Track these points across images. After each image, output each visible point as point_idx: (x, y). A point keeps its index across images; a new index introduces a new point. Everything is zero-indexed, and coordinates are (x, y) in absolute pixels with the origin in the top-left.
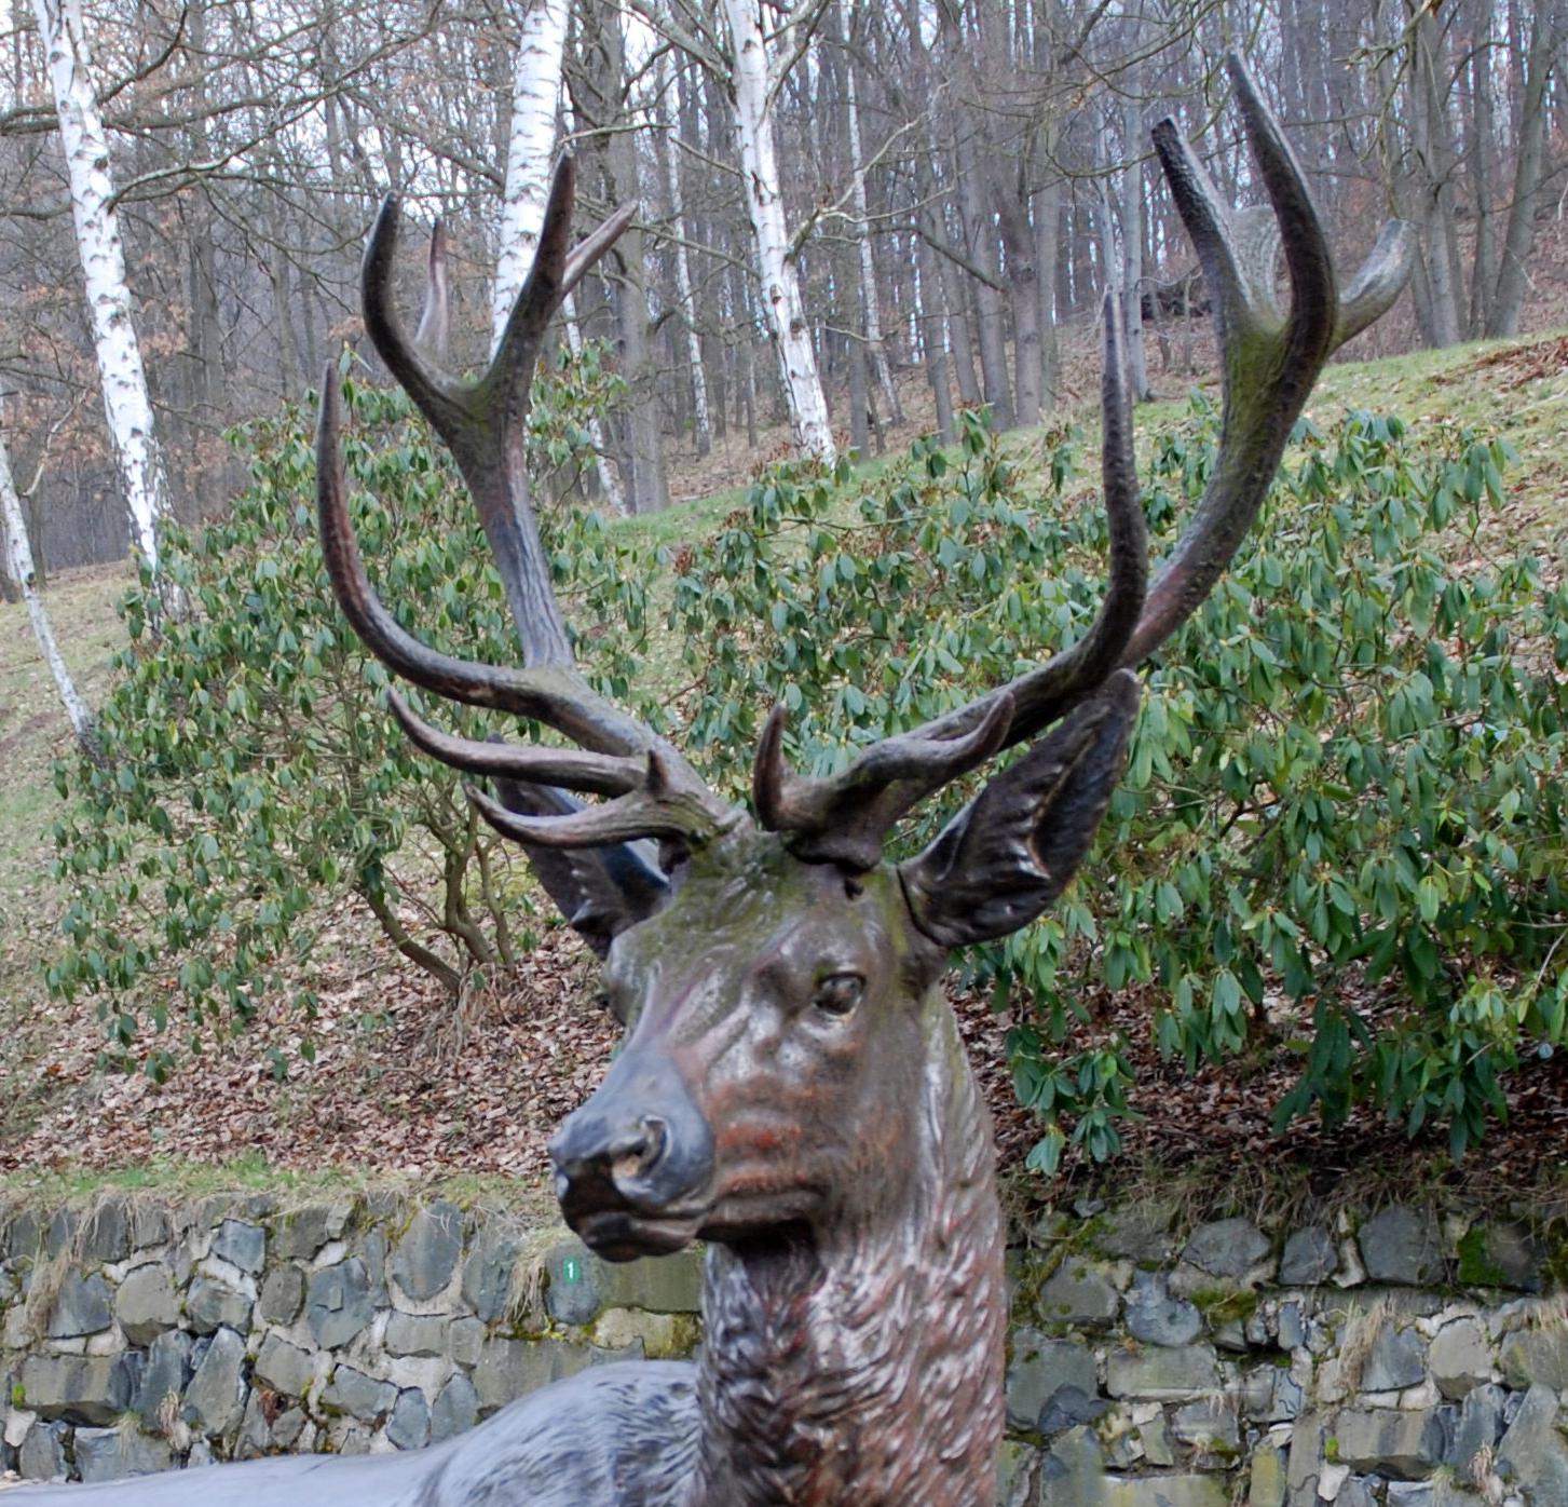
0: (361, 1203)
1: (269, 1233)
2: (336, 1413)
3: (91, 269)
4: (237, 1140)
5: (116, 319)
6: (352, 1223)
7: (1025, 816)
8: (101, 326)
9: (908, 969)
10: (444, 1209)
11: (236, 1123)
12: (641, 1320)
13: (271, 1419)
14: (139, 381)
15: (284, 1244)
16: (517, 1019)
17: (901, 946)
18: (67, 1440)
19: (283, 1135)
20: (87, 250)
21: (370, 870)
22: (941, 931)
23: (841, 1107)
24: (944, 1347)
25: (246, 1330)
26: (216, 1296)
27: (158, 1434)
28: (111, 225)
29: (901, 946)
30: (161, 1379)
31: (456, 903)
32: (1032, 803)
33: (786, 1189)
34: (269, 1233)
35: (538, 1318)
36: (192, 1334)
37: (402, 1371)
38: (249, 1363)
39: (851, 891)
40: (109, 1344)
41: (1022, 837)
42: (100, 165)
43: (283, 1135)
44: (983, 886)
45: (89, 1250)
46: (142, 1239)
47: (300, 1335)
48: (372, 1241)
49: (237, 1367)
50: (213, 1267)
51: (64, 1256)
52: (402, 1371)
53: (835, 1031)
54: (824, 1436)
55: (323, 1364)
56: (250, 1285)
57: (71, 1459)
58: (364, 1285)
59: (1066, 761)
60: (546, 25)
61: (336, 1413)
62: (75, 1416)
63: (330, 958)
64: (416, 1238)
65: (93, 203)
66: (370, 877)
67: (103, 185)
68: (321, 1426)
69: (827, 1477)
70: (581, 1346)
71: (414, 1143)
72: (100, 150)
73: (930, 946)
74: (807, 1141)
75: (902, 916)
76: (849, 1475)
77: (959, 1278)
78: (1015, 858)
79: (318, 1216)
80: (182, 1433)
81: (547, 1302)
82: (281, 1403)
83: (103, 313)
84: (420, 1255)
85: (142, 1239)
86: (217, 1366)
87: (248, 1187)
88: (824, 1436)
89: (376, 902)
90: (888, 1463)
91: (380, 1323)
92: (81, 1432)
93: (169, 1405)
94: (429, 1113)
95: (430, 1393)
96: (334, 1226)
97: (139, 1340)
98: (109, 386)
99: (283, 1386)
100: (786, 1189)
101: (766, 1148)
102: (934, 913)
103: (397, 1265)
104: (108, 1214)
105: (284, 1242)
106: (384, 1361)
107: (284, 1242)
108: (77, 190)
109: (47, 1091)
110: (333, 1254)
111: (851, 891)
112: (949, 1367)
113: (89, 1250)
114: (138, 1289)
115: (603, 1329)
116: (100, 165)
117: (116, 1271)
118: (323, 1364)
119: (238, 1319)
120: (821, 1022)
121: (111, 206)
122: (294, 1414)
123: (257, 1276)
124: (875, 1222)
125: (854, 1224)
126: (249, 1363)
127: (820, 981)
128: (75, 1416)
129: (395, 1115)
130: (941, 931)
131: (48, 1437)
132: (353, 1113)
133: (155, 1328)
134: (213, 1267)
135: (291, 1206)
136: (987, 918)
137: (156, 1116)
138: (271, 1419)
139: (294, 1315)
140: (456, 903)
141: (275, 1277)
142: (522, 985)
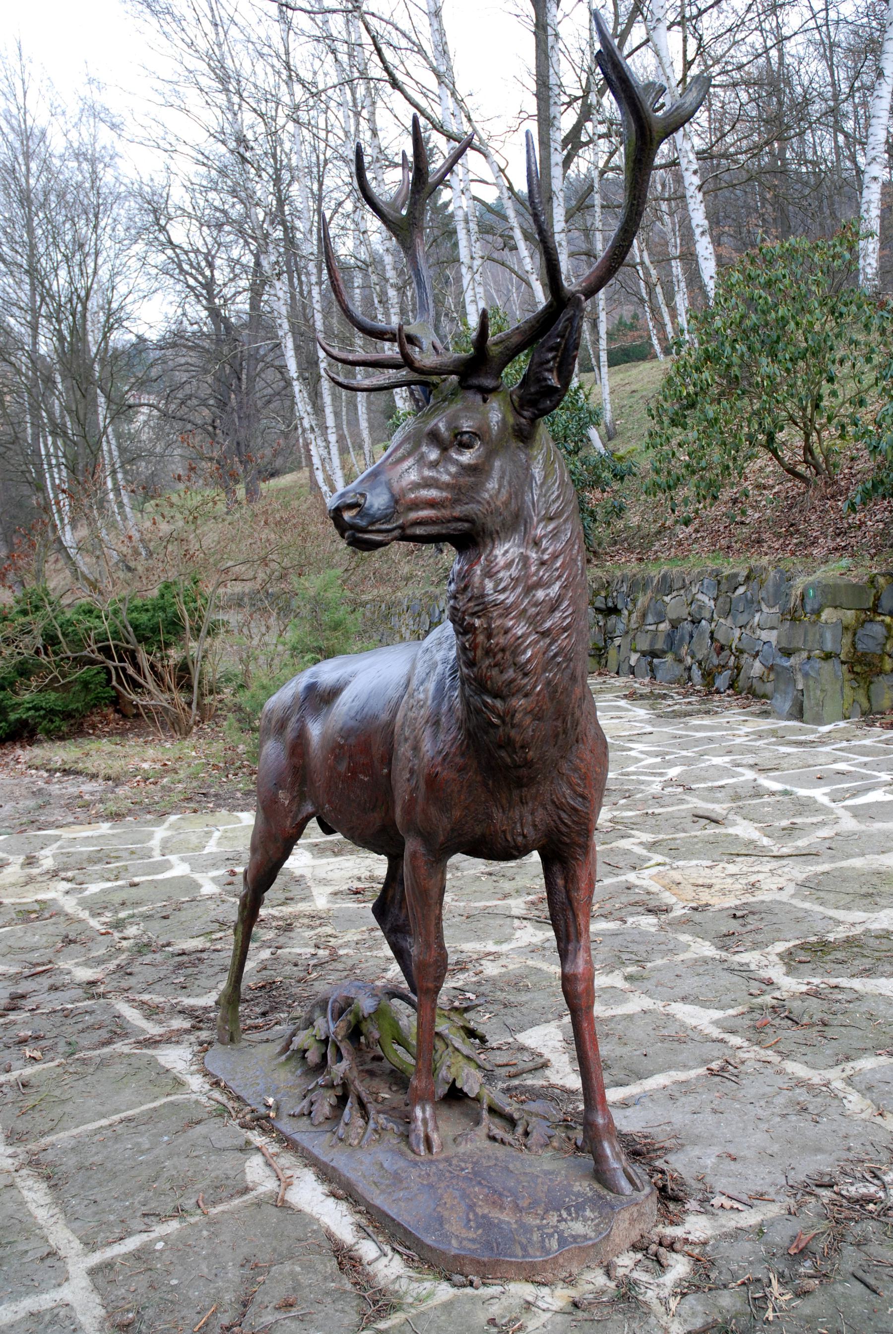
0: (751, 571)
1: (719, 582)
2: (742, 652)
3: (693, 214)
4: (721, 549)
5: (703, 233)
6: (748, 578)
7: (548, 362)
8: (697, 236)
9: (515, 430)
10: (780, 571)
11: (723, 542)
12: (840, 613)
13: (718, 654)
14: (713, 257)
15: (724, 587)
16: (833, 497)
17: (511, 420)
18: (650, 663)
19: (737, 546)
20: (691, 207)
21: (771, 438)
22: (526, 413)
23: (477, 487)
24: (539, 585)
25: (711, 620)
26: (701, 608)
27: (681, 661)
28: (700, 196)
29: (511, 420)
30: (682, 639)
31: (808, 449)
32: (550, 355)
33: (449, 521)
34: (719, 582)
35: (800, 612)
36: (693, 622)
37: (765, 635)
38: (712, 633)
39: (485, 400)
40: (664, 626)
41: (550, 370)
42: (695, 172)
43: (737, 546)
44: (536, 393)
45: (658, 591)
46: (676, 586)
47: (729, 622)
48: (754, 584)
49: (708, 635)
50: (700, 596)
51: (649, 594)
52: (765, 635)
53: (467, 457)
54: (477, 622)
55: (737, 633)
56: (712, 603)
57: (652, 671)
58: (752, 602)
59: (562, 337)
60: (884, 85)
61: (742, 652)
62: (654, 654)
63: (768, 477)
64: (770, 583)
65: (692, 188)
66: (770, 444)
67: (696, 180)
68: (737, 657)
69: (481, 638)
70: (815, 623)
71: (784, 547)
72: (695, 167)
73: (523, 421)
74: (456, 502)
75: (510, 408)
76: (489, 637)
77: (546, 557)
78: (545, 379)
79: (735, 575)
80: (689, 660)
81: (803, 606)
82: (722, 648)
83: (698, 231)
84: (771, 590)
85: (676, 586)
86: (701, 634)
87: (711, 565)
88: (477, 622)
89: (774, 452)
90: (506, 633)
91: (757, 616)
92: (655, 661)
93: (684, 650)
94: (792, 535)
95: (774, 643)
96: (741, 579)
97: (675, 625)
98: (701, 260)
99: (723, 642)
100: (449, 521)
101: (432, 504)
102: (522, 406)
103: (763, 594)
104: (664, 577)
105: (724, 585)
106: (758, 631)
107: (724, 585)
108: (687, 184)
109: (659, 532)
110: (741, 590)
111: (485, 400)
112: (540, 594)
113: (658, 591)
114: (674, 605)
115: (824, 616)
116: (695, 172)
117: (667, 599)
118: (737, 633)
119: (708, 616)
120: (461, 453)
121: (700, 188)
122: (727, 652)
123: (715, 599)
124: (502, 535)
125: (491, 535)
126: (712, 633)
127: (456, 436)
128: (654, 654)
129: (778, 536)
130: (526, 413)
131: (644, 662)
132: (764, 536)
133: (680, 620)
134: (700, 596)
135: (727, 572)
136: (541, 406)
137: (696, 540)
138: (718, 654)
139: (727, 614)
140: (808, 449)
141: (721, 600)
142: (836, 483)
